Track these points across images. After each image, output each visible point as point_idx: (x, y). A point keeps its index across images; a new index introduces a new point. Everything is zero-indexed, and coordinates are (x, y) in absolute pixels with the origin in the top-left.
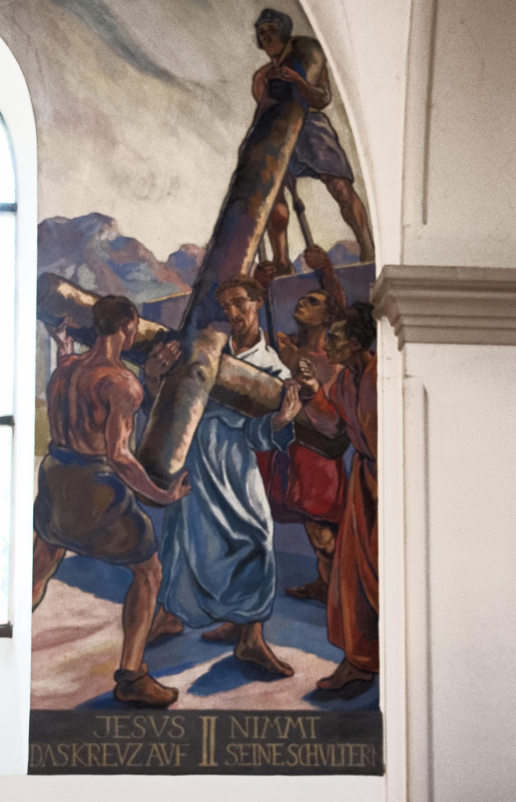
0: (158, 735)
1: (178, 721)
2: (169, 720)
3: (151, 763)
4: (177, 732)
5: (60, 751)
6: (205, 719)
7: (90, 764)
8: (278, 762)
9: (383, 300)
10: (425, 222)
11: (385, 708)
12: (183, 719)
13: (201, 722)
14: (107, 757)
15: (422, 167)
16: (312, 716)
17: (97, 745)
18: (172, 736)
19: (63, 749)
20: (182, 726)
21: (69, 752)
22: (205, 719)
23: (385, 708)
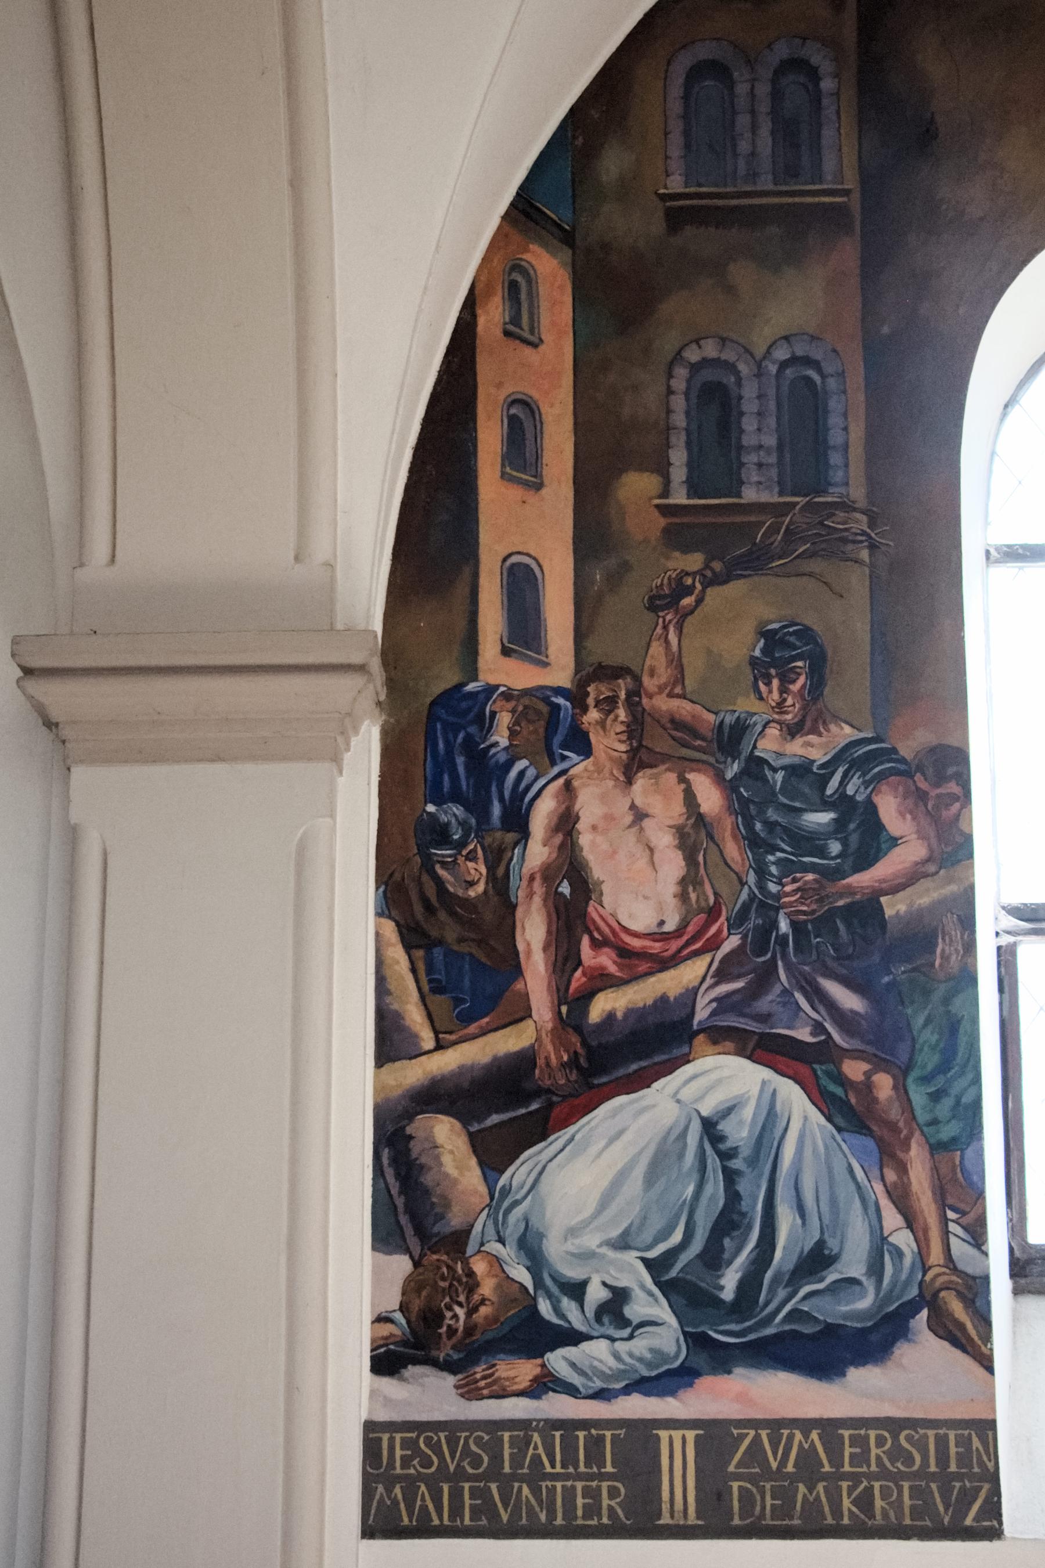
6: (664, 1434)
22: (664, 1434)
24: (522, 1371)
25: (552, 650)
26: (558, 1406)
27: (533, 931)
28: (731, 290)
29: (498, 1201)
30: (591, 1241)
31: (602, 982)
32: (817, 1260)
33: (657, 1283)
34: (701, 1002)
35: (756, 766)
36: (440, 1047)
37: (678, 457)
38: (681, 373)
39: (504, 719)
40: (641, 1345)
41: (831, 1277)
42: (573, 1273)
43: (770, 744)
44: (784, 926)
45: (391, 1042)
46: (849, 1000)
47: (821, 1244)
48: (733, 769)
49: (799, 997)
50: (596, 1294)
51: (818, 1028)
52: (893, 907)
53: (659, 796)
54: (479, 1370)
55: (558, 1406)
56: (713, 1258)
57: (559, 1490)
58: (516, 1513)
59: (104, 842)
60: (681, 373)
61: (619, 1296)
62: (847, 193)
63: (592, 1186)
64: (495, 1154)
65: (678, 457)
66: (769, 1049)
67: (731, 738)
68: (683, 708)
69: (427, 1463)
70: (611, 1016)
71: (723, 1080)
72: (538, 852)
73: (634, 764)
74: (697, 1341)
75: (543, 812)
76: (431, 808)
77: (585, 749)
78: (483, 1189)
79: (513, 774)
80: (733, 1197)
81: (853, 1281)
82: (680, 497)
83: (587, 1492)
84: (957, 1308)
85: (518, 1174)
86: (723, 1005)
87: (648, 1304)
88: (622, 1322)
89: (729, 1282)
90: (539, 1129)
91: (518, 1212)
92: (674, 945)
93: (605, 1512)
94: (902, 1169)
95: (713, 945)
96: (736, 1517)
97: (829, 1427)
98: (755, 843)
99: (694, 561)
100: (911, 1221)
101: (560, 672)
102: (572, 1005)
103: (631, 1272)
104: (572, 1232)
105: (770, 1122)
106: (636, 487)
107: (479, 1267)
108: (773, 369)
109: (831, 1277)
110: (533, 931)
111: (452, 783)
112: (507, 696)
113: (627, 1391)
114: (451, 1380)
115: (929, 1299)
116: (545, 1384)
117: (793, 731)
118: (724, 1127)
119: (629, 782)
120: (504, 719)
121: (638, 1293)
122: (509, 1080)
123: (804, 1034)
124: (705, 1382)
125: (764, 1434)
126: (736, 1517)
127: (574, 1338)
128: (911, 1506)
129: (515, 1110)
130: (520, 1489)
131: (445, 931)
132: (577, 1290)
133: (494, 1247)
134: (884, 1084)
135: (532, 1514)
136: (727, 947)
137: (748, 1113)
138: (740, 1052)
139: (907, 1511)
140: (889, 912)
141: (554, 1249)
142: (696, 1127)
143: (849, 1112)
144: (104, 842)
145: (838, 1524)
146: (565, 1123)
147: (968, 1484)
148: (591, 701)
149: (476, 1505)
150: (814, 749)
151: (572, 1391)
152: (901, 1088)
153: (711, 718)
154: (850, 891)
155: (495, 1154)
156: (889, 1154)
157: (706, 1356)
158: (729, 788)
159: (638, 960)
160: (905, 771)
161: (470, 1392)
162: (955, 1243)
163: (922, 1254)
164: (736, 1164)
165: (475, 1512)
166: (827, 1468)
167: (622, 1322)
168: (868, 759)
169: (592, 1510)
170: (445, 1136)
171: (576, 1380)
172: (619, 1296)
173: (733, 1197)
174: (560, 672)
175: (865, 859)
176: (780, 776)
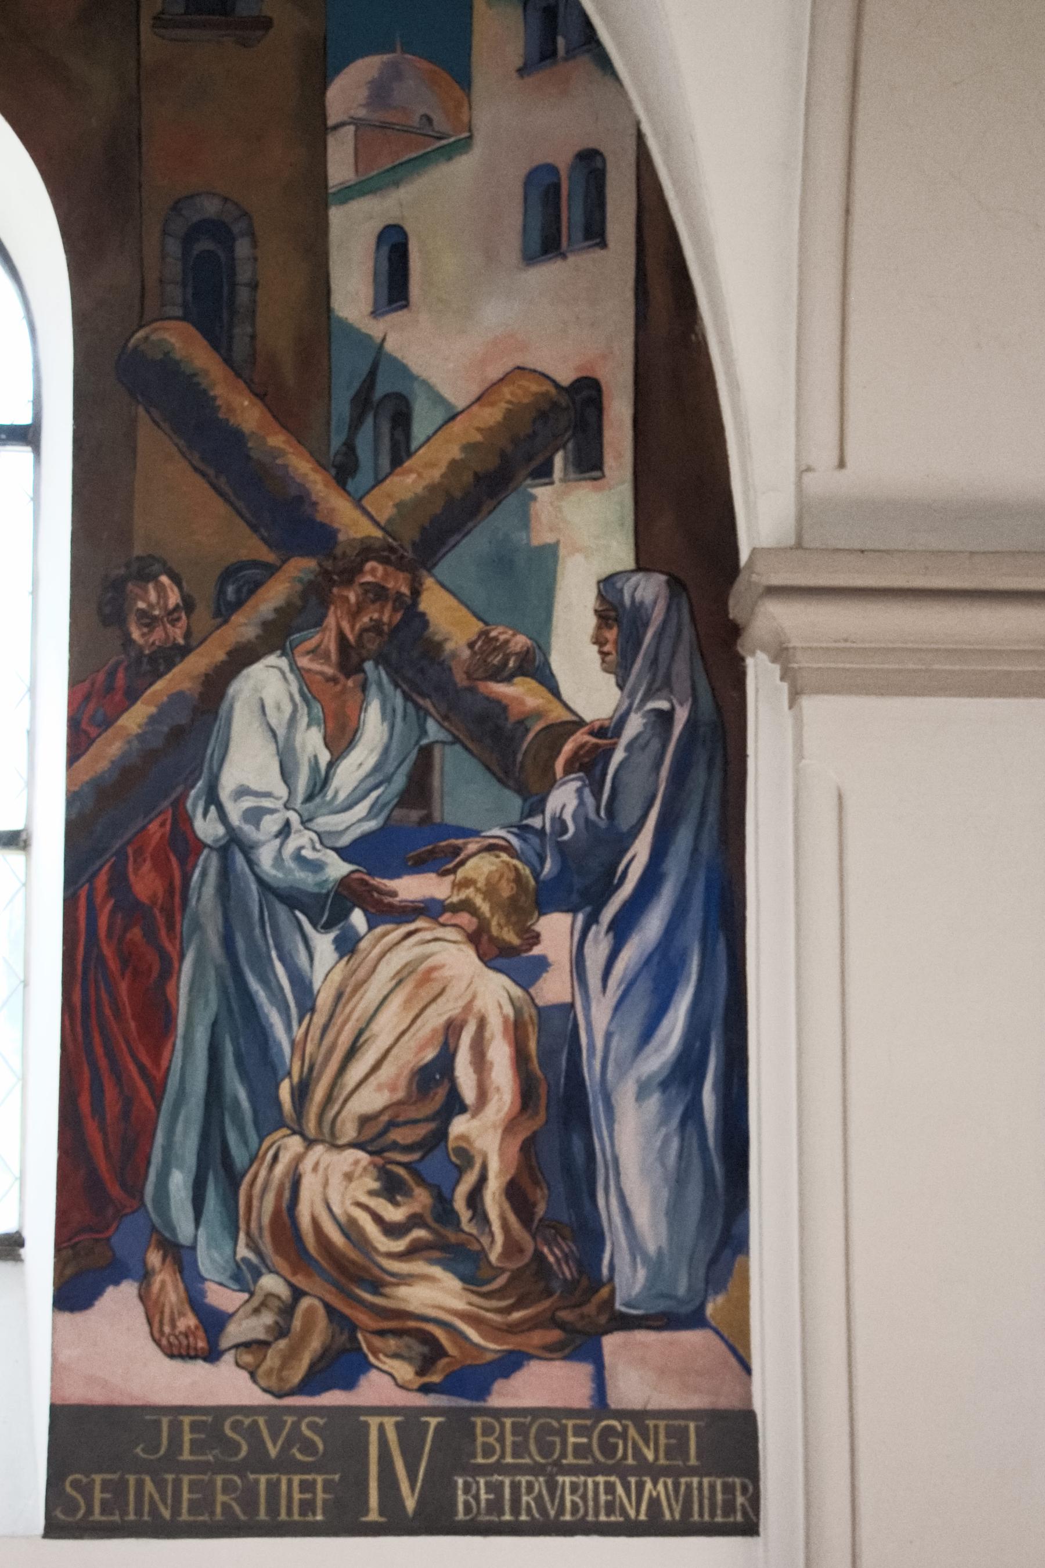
0: (273, 1452)
1: (312, 1426)
2: (296, 1425)
3: (112, 1514)
4: (308, 1447)
5: (68, 1489)
6: (374, 1422)
7: (219, 1516)
8: (103, 1512)
9: (301, 575)
10: (842, 464)
11: (764, 1405)
12: (321, 1421)
13: (366, 1426)
14: (191, 1501)
15: (838, 367)
16: (663, 1419)
17: (470, 1479)
18: (299, 1456)
19: (75, 1485)
20: (321, 1436)
21: (86, 1491)
22: (374, 1422)
23: (764, 1405)
28: (479, 429)
57: (262, 1486)
58: (687, 1511)
59: (509, 993)
83: (490, 1487)
93: (219, 1509)
96: (112, 1518)
125: (261, 1421)
126: (112, 1518)
128: (301, 1500)
130: (140, 1485)
135: (154, 1511)
139: (185, 1505)
144: (509, 993)
145: (517, 1520)
147: (680, 1463)
149: (306, 1500)
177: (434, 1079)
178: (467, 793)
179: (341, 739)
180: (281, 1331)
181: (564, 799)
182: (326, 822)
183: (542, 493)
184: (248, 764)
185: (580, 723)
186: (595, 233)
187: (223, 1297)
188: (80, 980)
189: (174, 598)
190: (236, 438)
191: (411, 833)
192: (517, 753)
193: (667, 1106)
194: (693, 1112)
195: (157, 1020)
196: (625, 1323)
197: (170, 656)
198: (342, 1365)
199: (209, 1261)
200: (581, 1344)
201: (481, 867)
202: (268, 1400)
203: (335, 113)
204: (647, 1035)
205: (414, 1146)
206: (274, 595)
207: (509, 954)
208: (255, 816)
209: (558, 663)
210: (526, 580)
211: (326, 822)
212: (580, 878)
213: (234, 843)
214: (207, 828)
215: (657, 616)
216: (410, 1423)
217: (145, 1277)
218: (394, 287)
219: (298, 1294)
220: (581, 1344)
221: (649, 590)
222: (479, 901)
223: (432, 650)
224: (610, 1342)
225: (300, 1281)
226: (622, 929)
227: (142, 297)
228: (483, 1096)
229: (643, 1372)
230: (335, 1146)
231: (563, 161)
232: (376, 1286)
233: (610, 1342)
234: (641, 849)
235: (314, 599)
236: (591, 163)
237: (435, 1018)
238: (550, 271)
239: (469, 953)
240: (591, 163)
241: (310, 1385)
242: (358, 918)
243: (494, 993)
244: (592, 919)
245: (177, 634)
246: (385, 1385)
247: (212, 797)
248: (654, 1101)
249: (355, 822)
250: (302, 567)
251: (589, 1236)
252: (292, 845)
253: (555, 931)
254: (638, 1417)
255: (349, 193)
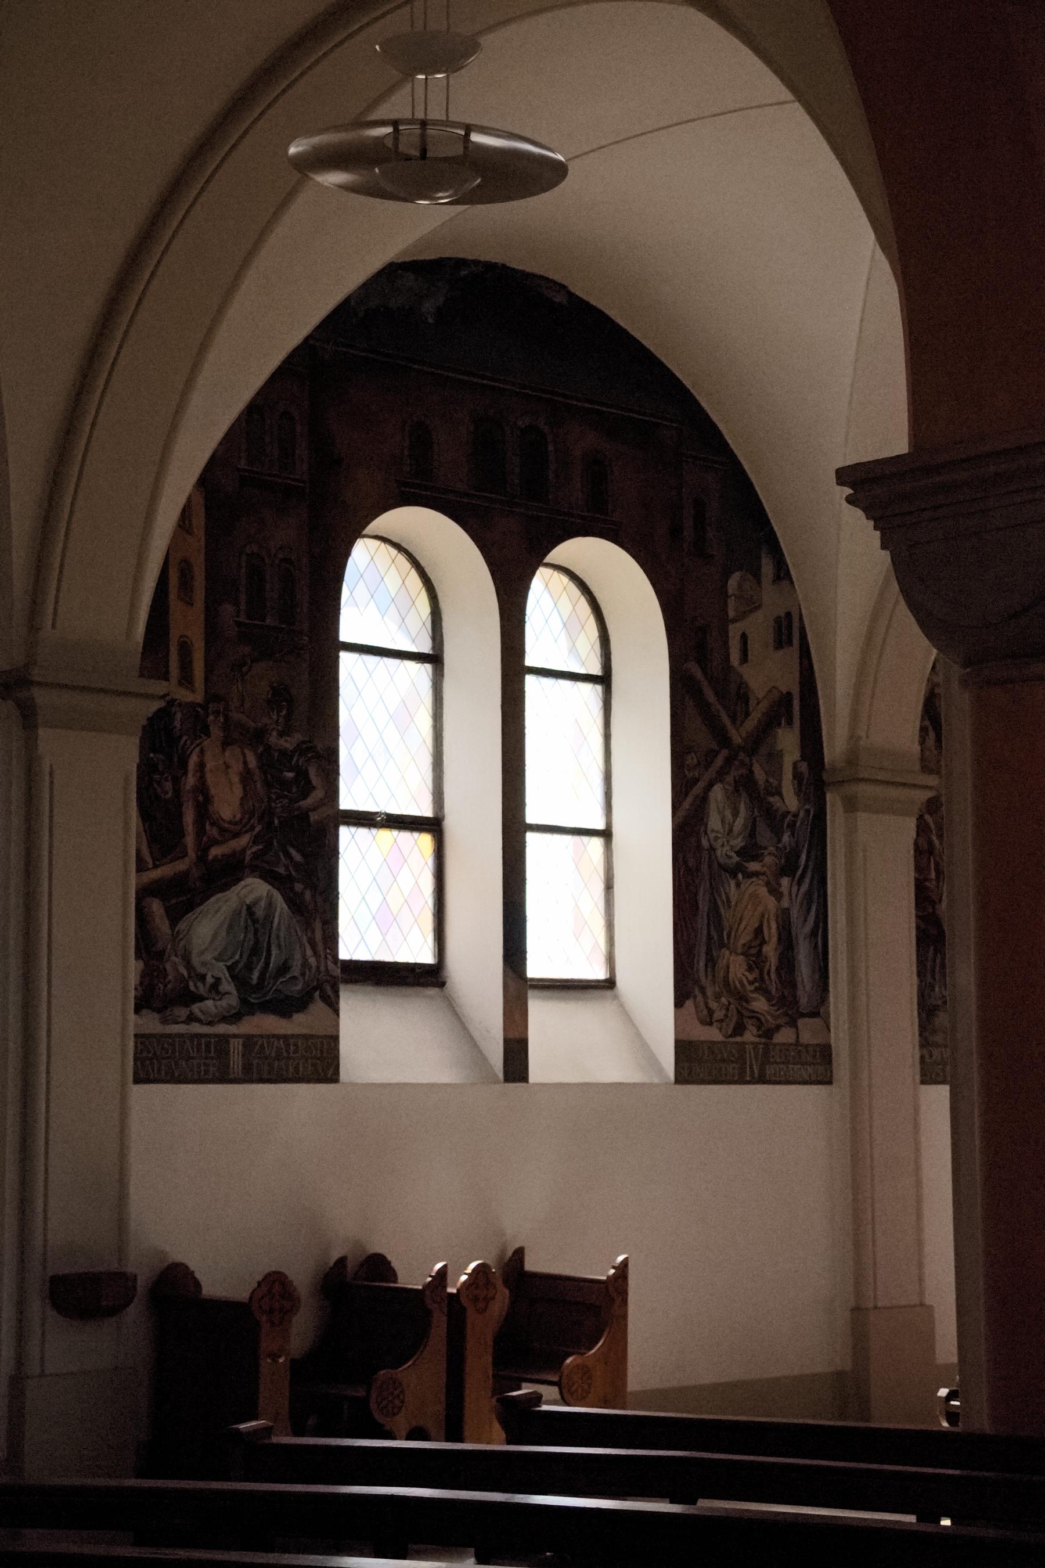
24: (182, 1012)
25: (197, 685)
26: (196, 1028)
27: (189, 818)
29: (175, 937)
30: (208, 957)
31: (215, 842)
32: (284, 968)
33: (231, 976)
34: (249, 852)
35: (268, 748)
36: (155, 867)
37: (243, 598)
38: (244, 558)
39: (179, 716)
40: (224, 1003)
41: (288, 976)
42: (202, 970)
43: (273, 739)
44: (276, 821)
45: (141, 867)
46: (298, 857)
47: (286, 961)
48: (261, 749)
49: (281, 854)
50: (210, 980)
51: (287, 868)
52: (314, 817)
53: (233, 756)
54: (168, 1012)
55: (196, 1028)
56: (249, 967)
60: (244, 558)
61: (218, 981)
62: (303, 482)
63: (208, 929)
64: (175, 916)
65: (243, 598)
66: (270, 877)
67: (258, 736)
68: (243, 718)
69: (149, 1052)
70: (216, 856)
71: (255, 888)
72: (191, 781)
73: (226, 743)
74: (243, 1001)
75: (194, 760)
76: (152, 755)
77: (208, 734)
78: (170, 932)
79: (182, 742)
80: (257, 942)
81: (294, 978)
82: (242, 619)
84: (328, 988)
85: (182, 926)
86: (256, 856)
87: (228, 986)
88: (218, 992)
89: (255, 975)
90: (190, 906)
91: (182, 943)
92: (238, 828)
94: (313, 931)
95: (253, 828)
97: (285, 1037)
98: (268, 785)
99: (247, 650)
100: (315, 953)
101: (198, 697)
102: (203, 850)
103: (220, 970)
104: (202, 953)
105: (270, 905)
106: (227, 609)
107: (168, 967)
108: (277, 562)
109: (288, 976)
110: (189, 818)
111: (163, 746)
112: (180, 705)
113: (219, 1021)
114: (156, 1016)
115: (319, 987)
116: (191, 1019)
117: (281, 735)
118: (254, 909)
119: (224, 750)
120: (179, 716)
121: (224, 980)
122: (178, 882)
123: (281, 870)
124: (246, 1018)
127: (202, 999)
129: (180, 896)
131: (160, 816)
132: (203, 978)
133: (173, 958)
134: (308, 895)
136: (257, 829)
137: (263, 904)
138: (261, 877)
140: (312, 819)
141: (196, 961)
142: (245, 908)
143: (295, 905)
146: (200, 904)
148: (210, 710)
150: (288, 744)
151: (199, 1021)
152: (313, 896)
153: (253, 724)
154: (299, 808)
155: (175, 916)
156: (308, 926)
157: (246, 1009)
158: (259, 757)
159: (228, 833)
160: (318, 756)
161: (165, 1021)
162: (329, 963)
163: (318, 967)
164: (257, 926)
165: (166, 1074)
166: (285, 1054)
167: (218, 992)
168: (306, 749)
169: (207, 1072)
170: (156, 907)
171: (202, 1017)
172: (218, 981)
173: (257, 942)
174: (198, 697)
175: (305, 797)
176: (276, 754)
177: (759, 931)
178: (765, 836)
179: (736, 814)
180: (726, 1016)
181: (786, 838)
182: (732, 843)
183: (780, 731)
184: (714, 822)
185: (789, 812)
186: (790, 643)
187: (713, 1005)
188: (705, 683)
189: (695, 761)
190: (708, 705)
191: (750, 851)
192: (775, 820)
193: (810, 942)
194: (816, 947)
195: (695, 906)
196: (803, 1015)
197: (696, 781)
198: (739, 1029)
199: (709, 992)
200: (793, 1023)
201: (768, 860)
202: (724, 1039)
203: (730, 592)
204: (805, 921)
205: (756, 961)
206: (719, 761)
207: (775, 892)
208: (716, 838)
209: (784, 791)
210: (775, 757)
211: (733, 842)
212: (788, 868)
213: (712, 849)
214: (705, 843)
215: (806, 776)
216: (755, 1045)
217: (695, 997)
218: (744, 658)
219: (730, 1003)
220: (793, 1023)
221: (804, 767)
222: (768, 873)
223: (755, 783)
224: (801, 1022)
225: (731, 1000)
226: (799, 884)
227: (759, 107)
228: (770, 938)
229: (808, 1031)
230: (737, 954)
231: (782, 614)
232: (747, 1002)
233: (801, 1022)
234: (804, 857)
235: (729, 761)
236: (789, 615)
237: (760, 909)
238: (781, 652)
239: (765, 889)
240: (789, 615)
241: (731, 1036)
242: (740, 876)
243: (771, 902)
244: (793, 881)
245: (697, 774)
246: (750, 1036)
247: (706, 832)
248: (808, 940)
249: (738, 842)
250: (725, 752)
251: (793, 985)
252: (725, 850)
253: (785, 881)
254: (807, 1046)
255: (734, 621)
